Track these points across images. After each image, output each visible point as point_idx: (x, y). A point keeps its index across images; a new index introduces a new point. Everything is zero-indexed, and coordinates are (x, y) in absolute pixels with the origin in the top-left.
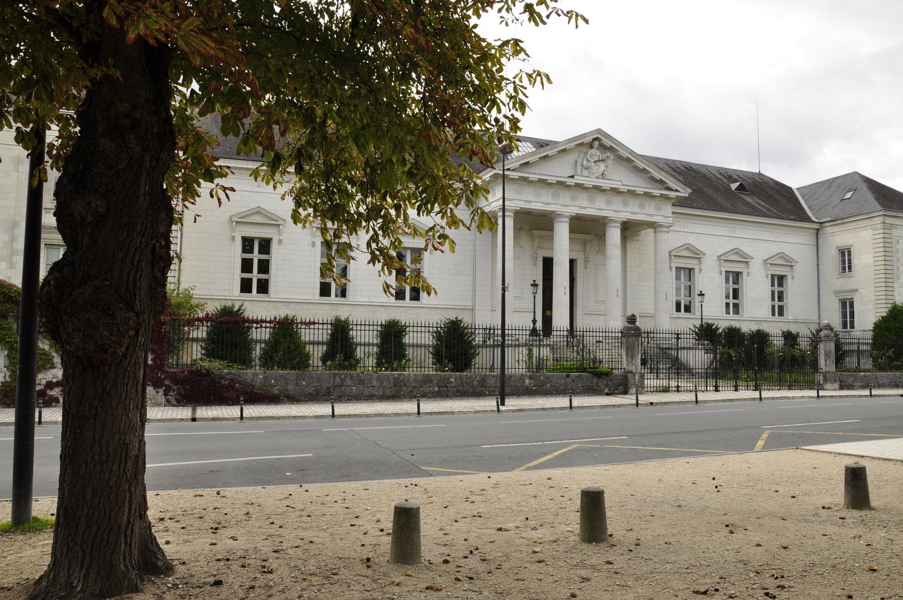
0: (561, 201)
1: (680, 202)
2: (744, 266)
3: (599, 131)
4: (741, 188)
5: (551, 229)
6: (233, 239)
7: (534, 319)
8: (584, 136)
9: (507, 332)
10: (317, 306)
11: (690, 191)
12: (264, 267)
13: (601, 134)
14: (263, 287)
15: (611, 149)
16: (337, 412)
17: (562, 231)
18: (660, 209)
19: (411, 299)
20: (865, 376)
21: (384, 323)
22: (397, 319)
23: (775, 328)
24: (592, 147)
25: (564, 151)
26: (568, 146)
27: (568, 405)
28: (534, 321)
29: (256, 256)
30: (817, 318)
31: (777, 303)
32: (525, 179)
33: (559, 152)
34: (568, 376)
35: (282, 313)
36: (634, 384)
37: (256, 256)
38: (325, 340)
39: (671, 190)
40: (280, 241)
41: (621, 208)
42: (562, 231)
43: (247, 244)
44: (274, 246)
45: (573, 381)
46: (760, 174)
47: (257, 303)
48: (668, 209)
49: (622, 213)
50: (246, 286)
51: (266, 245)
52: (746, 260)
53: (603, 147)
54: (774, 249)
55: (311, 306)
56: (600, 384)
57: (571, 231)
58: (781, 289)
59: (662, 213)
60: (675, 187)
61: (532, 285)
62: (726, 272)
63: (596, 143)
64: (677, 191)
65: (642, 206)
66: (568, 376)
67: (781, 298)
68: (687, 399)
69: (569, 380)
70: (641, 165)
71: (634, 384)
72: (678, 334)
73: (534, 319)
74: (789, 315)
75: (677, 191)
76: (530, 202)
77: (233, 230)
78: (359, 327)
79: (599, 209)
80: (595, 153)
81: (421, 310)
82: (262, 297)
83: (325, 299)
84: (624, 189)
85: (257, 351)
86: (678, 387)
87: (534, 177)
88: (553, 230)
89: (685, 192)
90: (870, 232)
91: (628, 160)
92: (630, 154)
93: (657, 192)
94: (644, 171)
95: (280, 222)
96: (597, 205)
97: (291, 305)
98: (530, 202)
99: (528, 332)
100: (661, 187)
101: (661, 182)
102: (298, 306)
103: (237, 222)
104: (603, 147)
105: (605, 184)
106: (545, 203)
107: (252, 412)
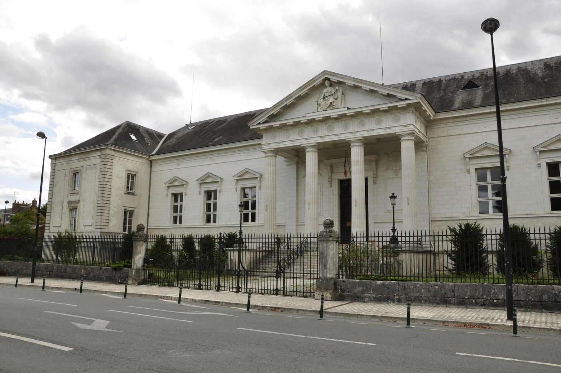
0: (305, 136)
3: (325, 72)
7: (394, 227)
8: (313, 80)
9: (370, 239)
10: (536, 219)
13: (328, 74)
15: (340, 83)
17: (357, 154)
18: (398, 120)
20: (383, 285)
21: (552, 230)
22: (208, 234)
23: (176, 233)
27: (79, 287)
31: (212, 213)
32: (271, 128)
34: (101, 268)
35: (187, 233)
36: (132, 277)
39: (401, 100)
41: (376, 127)
42: (357, 154)
45: (103, 272)
49: (359, 133)
55: (198, 229)
56: (116, 276)
60: (404, 96)
61: (391, 197)
64: (407, 99)
65: (379, 122)
66: (101, 268)
67: (175, 208)
69: (101, 272)
71: (132, 277)
73: (394, 227)
74: (220, 221)
75: (407, 99)
76: (282, 142)
78: (440, 238)
79: (337, 135)
80: (328, 90)
81: (254, 228)
84: (367, 110)
85: (492, 260)
90: (99, 160)
92: (355, 81)
95: (258, 175)
99: (388, 239)
102: (193, 230)
103: (470, 158)
105: (333, 113)
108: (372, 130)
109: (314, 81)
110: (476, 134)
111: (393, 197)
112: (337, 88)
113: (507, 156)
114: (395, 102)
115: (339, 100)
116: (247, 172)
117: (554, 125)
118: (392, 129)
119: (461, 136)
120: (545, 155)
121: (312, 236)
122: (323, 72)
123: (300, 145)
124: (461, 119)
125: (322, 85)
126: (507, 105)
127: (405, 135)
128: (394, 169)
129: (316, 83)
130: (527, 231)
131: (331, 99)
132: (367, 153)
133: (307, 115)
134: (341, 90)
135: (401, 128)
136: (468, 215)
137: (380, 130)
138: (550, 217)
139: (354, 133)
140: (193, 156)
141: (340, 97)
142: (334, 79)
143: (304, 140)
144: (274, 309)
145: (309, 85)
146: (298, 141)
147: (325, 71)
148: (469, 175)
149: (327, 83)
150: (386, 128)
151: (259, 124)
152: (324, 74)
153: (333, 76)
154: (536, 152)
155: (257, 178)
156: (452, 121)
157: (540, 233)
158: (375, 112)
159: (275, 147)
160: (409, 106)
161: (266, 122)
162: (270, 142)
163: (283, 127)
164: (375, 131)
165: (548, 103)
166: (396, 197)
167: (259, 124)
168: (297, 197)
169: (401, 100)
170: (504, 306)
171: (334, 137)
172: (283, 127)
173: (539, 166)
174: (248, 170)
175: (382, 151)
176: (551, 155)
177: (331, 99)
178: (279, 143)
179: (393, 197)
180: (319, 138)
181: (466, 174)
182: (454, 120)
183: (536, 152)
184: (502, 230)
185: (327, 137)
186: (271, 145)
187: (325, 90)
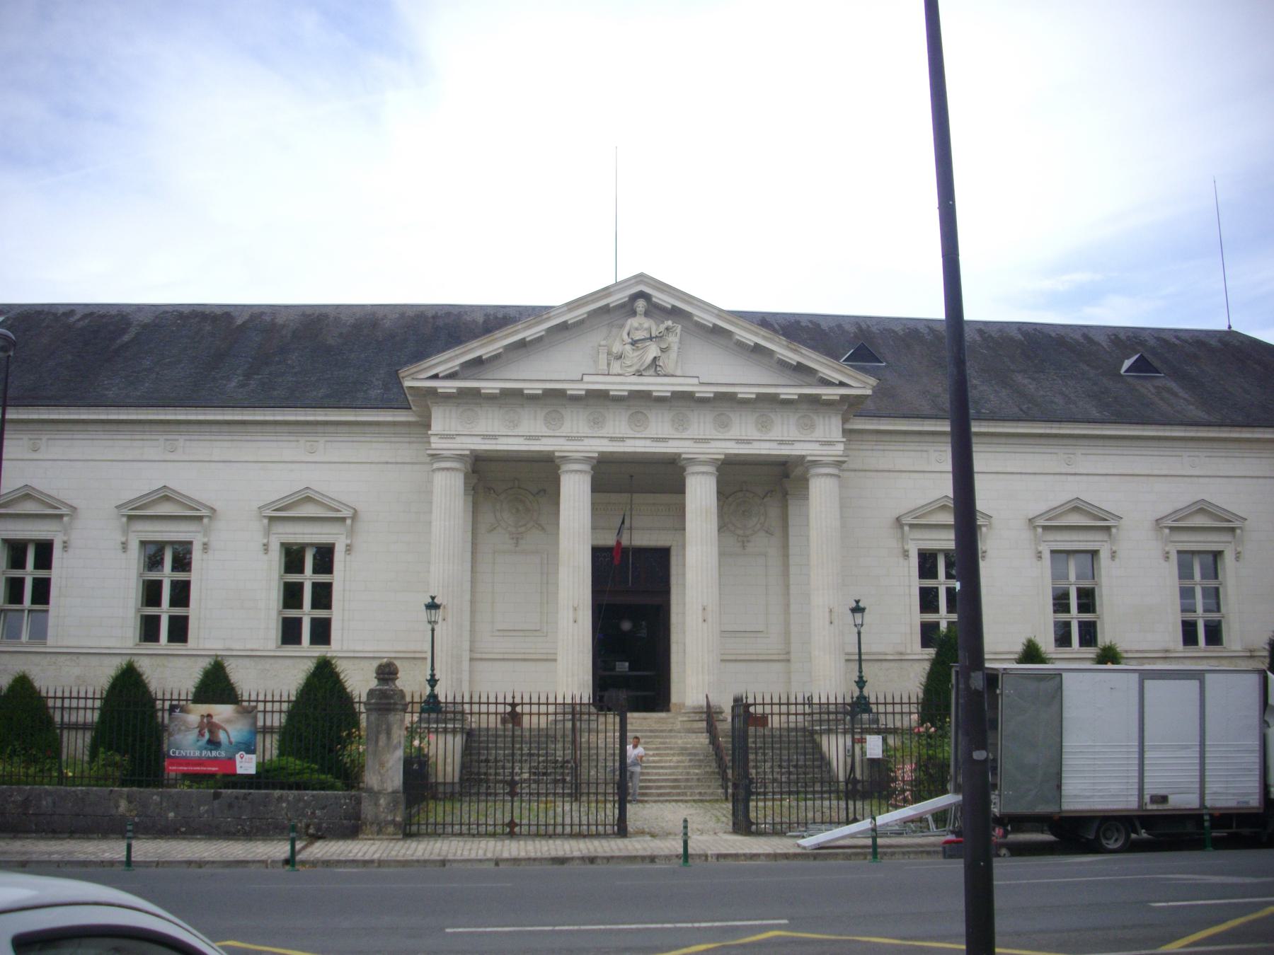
1: (851, 407)
2: (1099, 536)
3: (641, 278)
4: (1142, 366)
6: (125, 546)
8: (606, 292)
11: (872, 381)
12: (323, 596)
14: (179, 630)
15: (674, 312)
16: (136, 857)
17: (701, 493)
18: (813, 427)
19: (1081, 644)
24: (634, 313)
26: (571, 317)
29: (308, 578)
32: (476, 393)
37: (167, 575)
38: (276, 724)
39: (826, 383)
41: (757, 435)
42: (701, 493)
43: (293, 558)
44: (196, 555)
46: (1230, 333)
47: (288, 662)
48: (830, 429)
49: (713, 444)
50: (149, 630)
51: (44, 553)
52: (1104, 525)
53: (655, 310)
54: (1180, 495)
57: (597, 488)
58: (42, 574)
59: (815, 439)
60: (836, 376)
62: (1179, 552)
63: (641, 305)
64: (842, 384)
65: (764, 425)
68: (107, 856)
70: (750, 337)
72: (513, 705)
73: (433, 675)
75: (842, 384)
76: (622, 439)
77: (125, 532)
80: (640, 325)
82: (177, 648)
83: (290, 650)
84: (707, 392)
86: (512, 824)
88: (683, 492)
89: (860, 385)
91: (716, 331)
92: (719, 317)
93: (790, 392)
95: (345, 513)
97: (82, 658)
101: (800, 369)
104: (655, 310)
105: (659, 385)
107: (638, 846)
108: (748, 442)
109: (609, 295)
110: (921, 475)
111: (858, 609)
113: (984, 529)
114: (810, 385)
115: (673, 354)
116: (308, 499)
117: (1064, 477)
118: (797, 445)
120: (1051, 536)
122: (635, 277)
123: (553, 452)
125: (628, 308)
126: (991, 423)
128: (740, 532)
129: (614, 300)
130: (44, 694)
131: (653, 351)
133: (586, 378)
135: (816, 446)
137: (767, 445)
138: (503, 660)
139: (702, 442)
140: (99, 427)
141: (675, 347)
143: (562, 441)
144: (775, 856)
145: (593, 301)
147: (641, 275)
149: (641, 305)
151: (435, 377)
152: (638, 283)
153: (662, 291)
154: (1035, 527)
155: (344, 519)
157: (480, 703)
159: (473, 447)
160: (844, 398)
164: (756, 445)
165: (1062, 432)
167: (435, 377)
169: (826, 383)
170: (960, 857)
171: (648, 443)
173: (1039, 556)
174: (311, 494)
176: (1059, 536)
177: (653, 351)
178: (485, 437)
179: (858, 609)
180: (605, 442)
181: (901, 560)
183: (1035, 527)
184: (921, 695)
186: (459, 439)
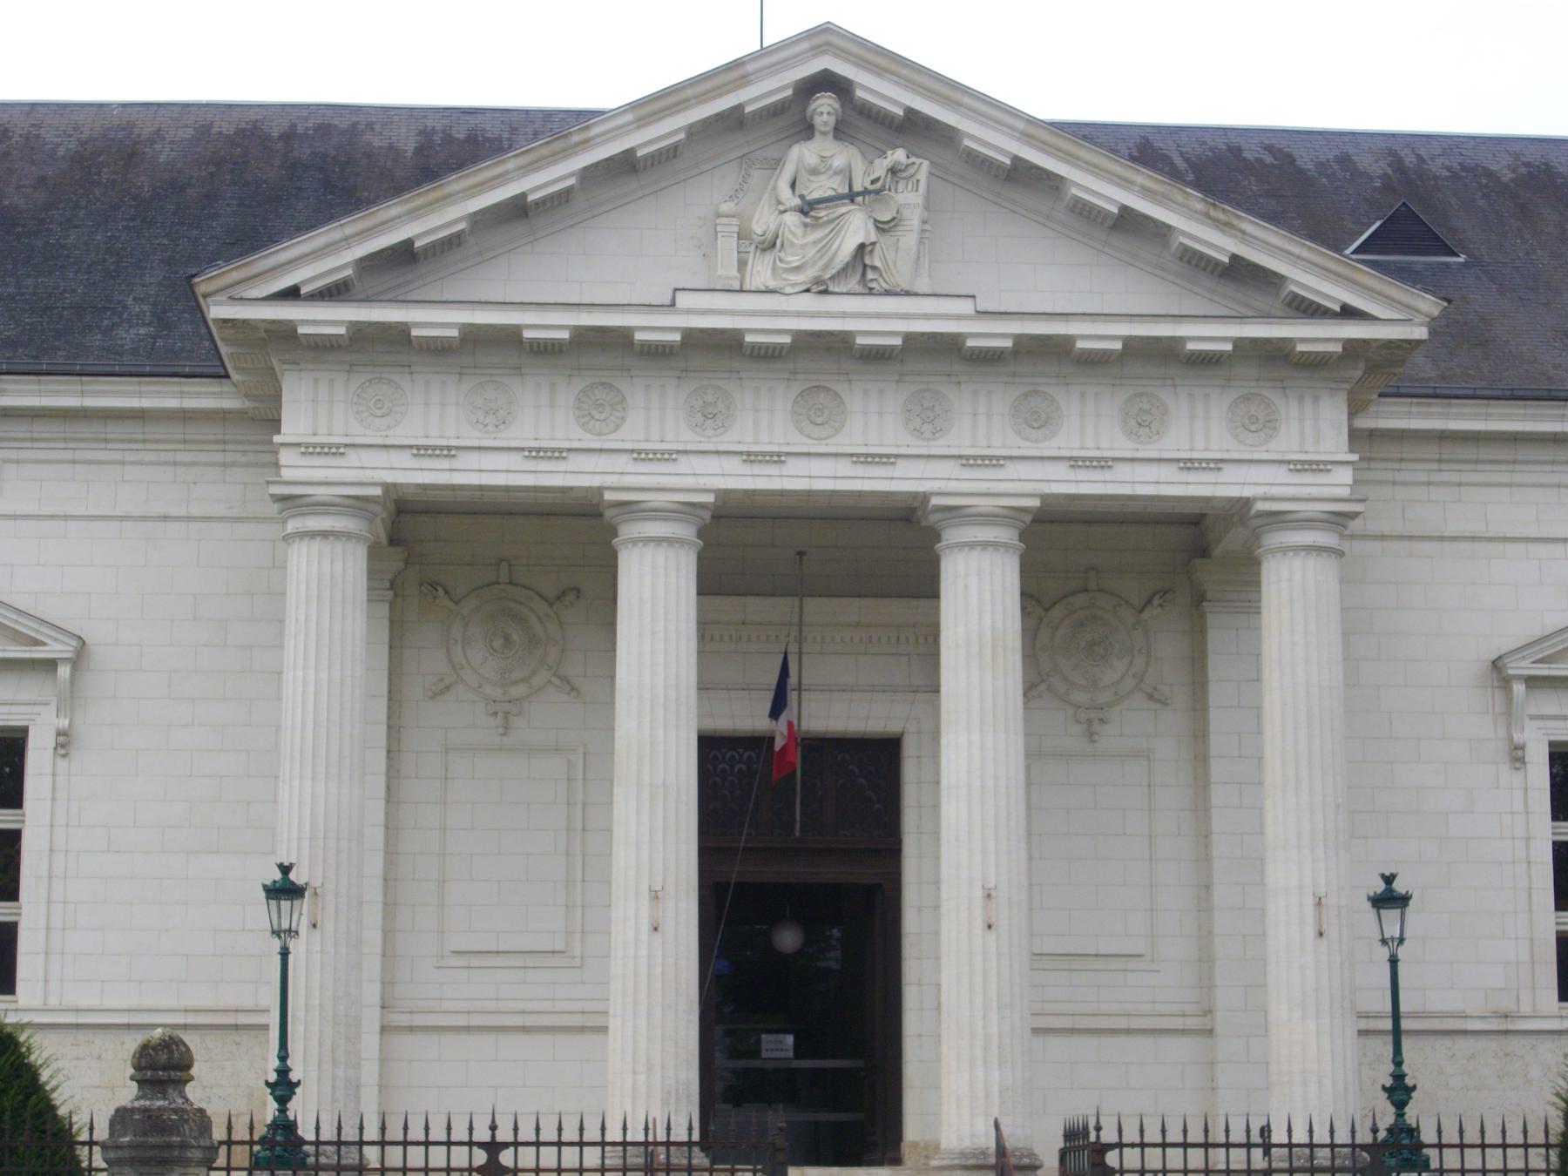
3: (825, 37)
5: (922, 584)
8: (735, 72)
11: (1430, 305)
15: (913, 128)
17: (979, 598)
18: (1269, 425)
24: (807, 130)
25: (626, 166)
26: (644, 140)
28: (690, 1129)
30: (599, 1132)
32: (397, 339)
33: (590, 175)
39: (1308, 309)
40: (64, 742)
41: (1124, 447)
42: (979, 598)
48: (1317, 428)
49: (1013, 470)
53: (864, 123)
59: (1269, 457)
60: (1335, 293)
64: (1348, 313)
65: (1143, 422)
75: (1348, 313)
80: (822, 160)
87: (432, 319)
89: (1398, 314)
91: (1021, 175)
92: (1028, 138)
94: (1127, 222)
95: (55, 648)
96: (853, 438)
98: (448, 451)
100: (1262, 301)
101: (1239, 272)
104: (864, 123)
105: (872, 319)
106: (537, 453)
109: (744, 81)
111: (1389, 899)
112: (899, 155)
115: (908, 238)
118: (1230, 473)
119: (1480, 547)
121: (1515, 1136)
124: (1485, 452)
125: (791, 117)
127: (1309, 523)
128: (1081, 697)
129: (757, 94)
131: (856, 228)
132: (1039, 599)
133: (684, 300)
134: (922, 176)
136: (1507, 1004)
137: (1153, 472)
139: (982, 463)
141: (913, 219)
142: (873, 88)
143: (621, 463)
145: (702, 98)
146: (576, 462)
147: (827, 30)
148: (1517, 779)
149: (825, 107)
150: (1188, 465)
151: (292, 294)
155: (50, 665)
156: (1431, 451)
158: (1155, 361)
159: (389, 477)
161: (334, 292)
162: (363, 440)
163: (492, 351)
164: (1122, 471)
166: (1402, 901)
167: (292, 294)
168: (391, 828)
169: (1308, 309)
171: (845, 467)
172: (492, 351)
175: (1138, 590)
179: (1389, 899)
181: (1505, 769)
182: (1449, 450)
185: (794, 466)
186: (353, 458)
187: (804, 154)
